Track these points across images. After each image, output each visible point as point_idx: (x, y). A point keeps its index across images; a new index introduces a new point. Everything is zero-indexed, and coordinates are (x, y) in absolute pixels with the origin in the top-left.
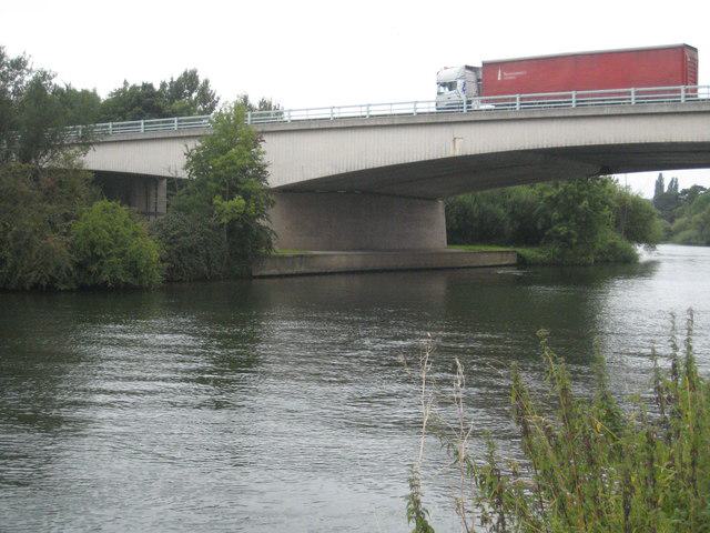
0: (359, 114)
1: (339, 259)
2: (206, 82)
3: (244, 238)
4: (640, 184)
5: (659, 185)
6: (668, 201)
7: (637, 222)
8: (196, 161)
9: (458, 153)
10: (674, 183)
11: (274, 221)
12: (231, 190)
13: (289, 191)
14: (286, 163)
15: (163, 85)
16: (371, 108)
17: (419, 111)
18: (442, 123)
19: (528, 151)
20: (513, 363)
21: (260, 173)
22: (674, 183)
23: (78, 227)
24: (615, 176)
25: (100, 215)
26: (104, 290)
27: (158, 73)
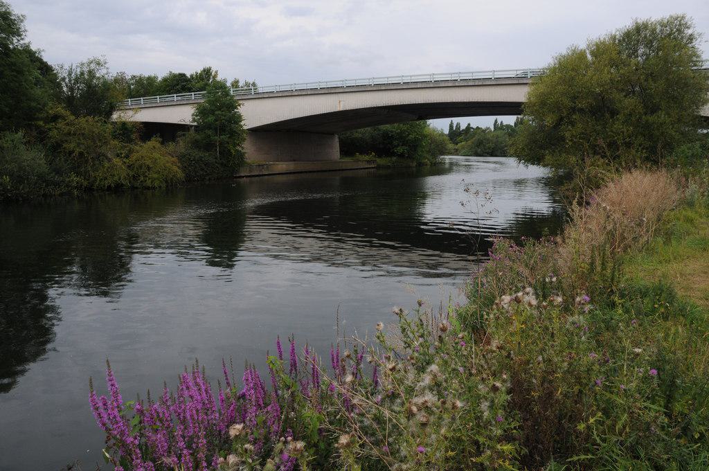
0: (429, 80)
1: (282, 166)
2: (216, 72)
3: (231, 161)
4: (440, 125)
5: (451, 126)
6: (455, 134)
7: (439, 146)
8: (202, 112)
9: (341, 109)
10: (458, 125)
11: (249, 149)
12: (222, 129)
13: (255, 131)
14: (253, 115)
15: (192, 76)
16: (495, 73)
17: (496, 77)
18: (333, 93)
19: (378, 107)
20: (11, 46)
21: (238, 118)
22: (458, 125)
23: (134, 156)
24: (430, 122)
25: (150, 151)
26: (143, 196)
27: (191, 68)
